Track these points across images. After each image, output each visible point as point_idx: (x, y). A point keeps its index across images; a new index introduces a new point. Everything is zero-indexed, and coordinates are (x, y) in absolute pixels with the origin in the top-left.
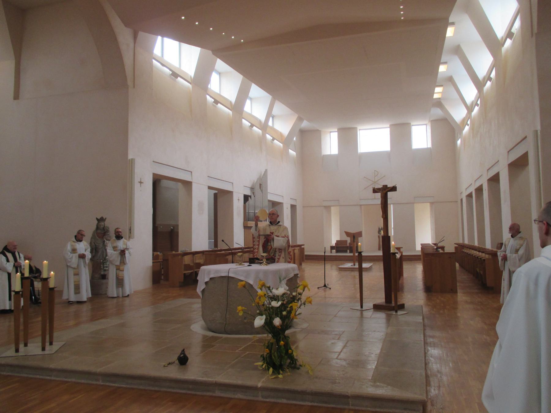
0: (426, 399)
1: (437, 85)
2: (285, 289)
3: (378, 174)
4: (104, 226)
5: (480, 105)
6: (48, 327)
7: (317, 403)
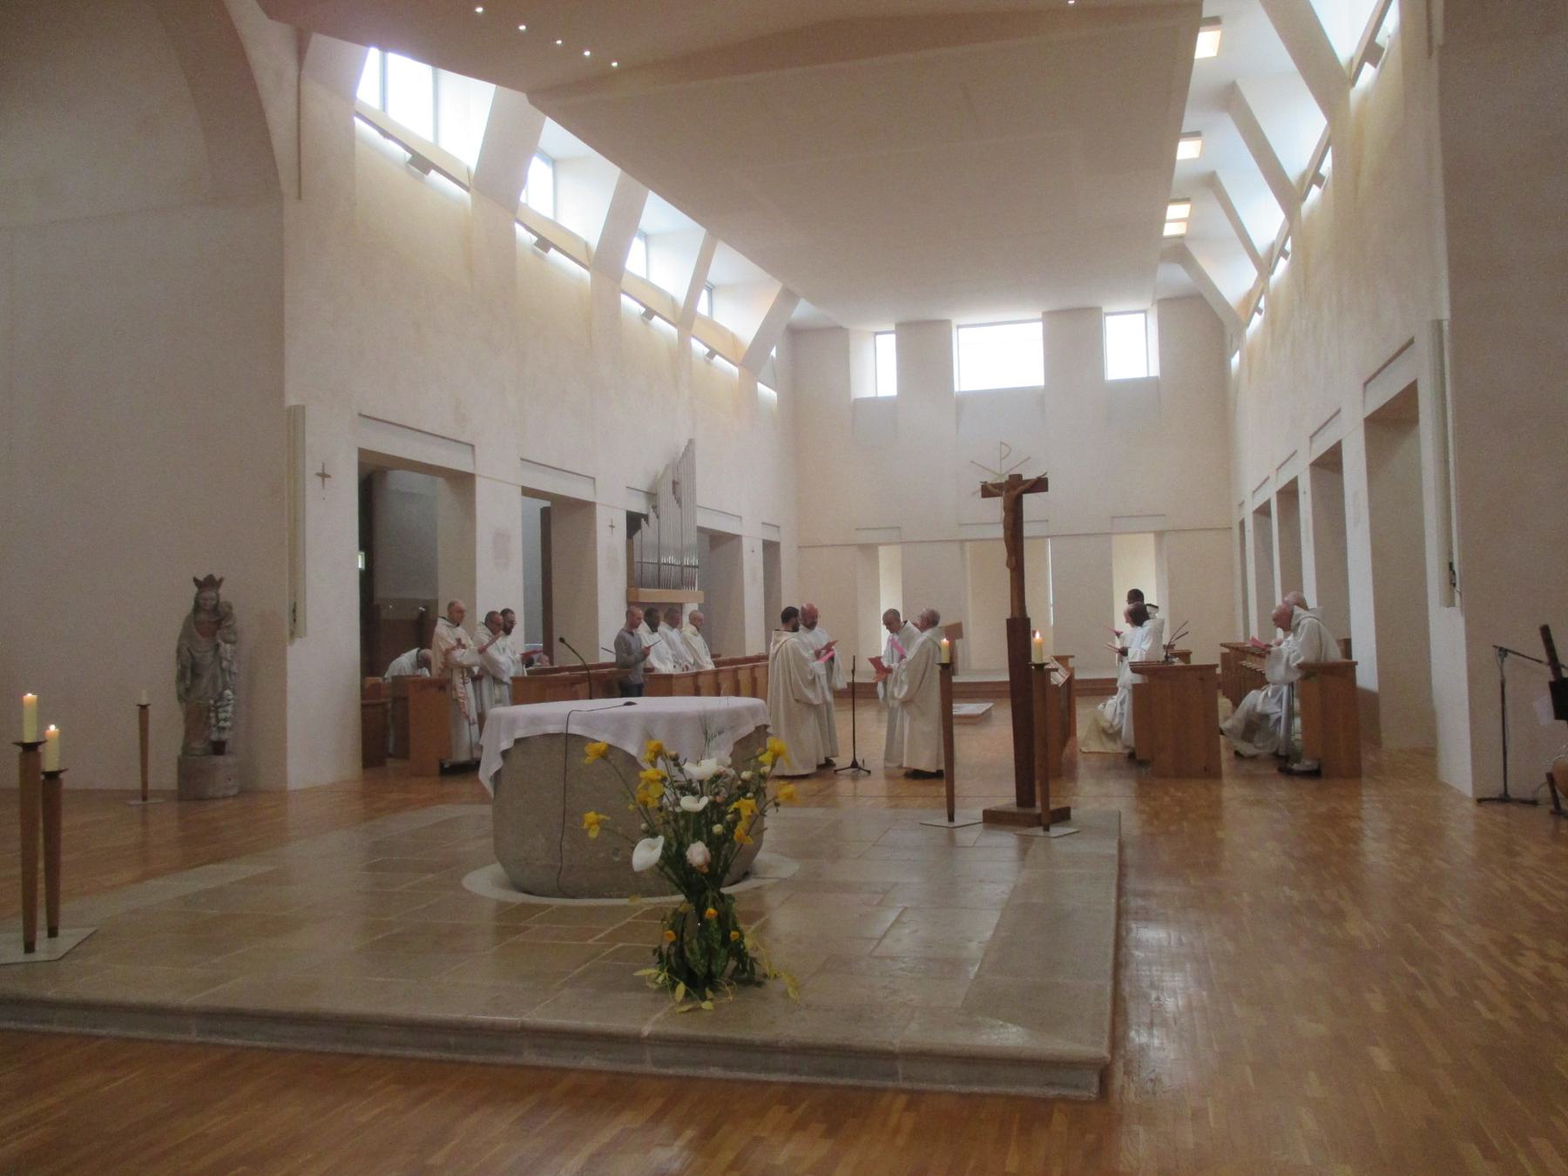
0: (1108, 1056)
2: (720, 762)
4: (218, 602)
7: (808, 1074)
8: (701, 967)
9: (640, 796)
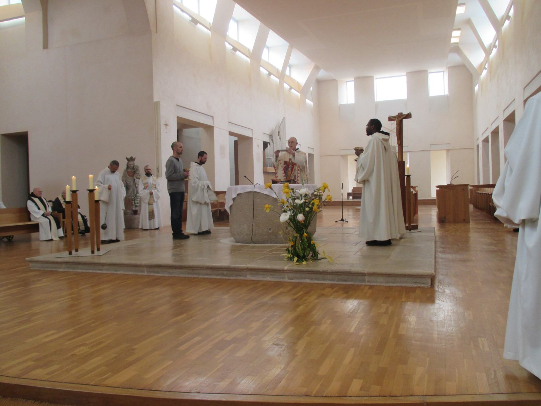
4: (134, 165)
5: (497, 47)
7: (337, 281)
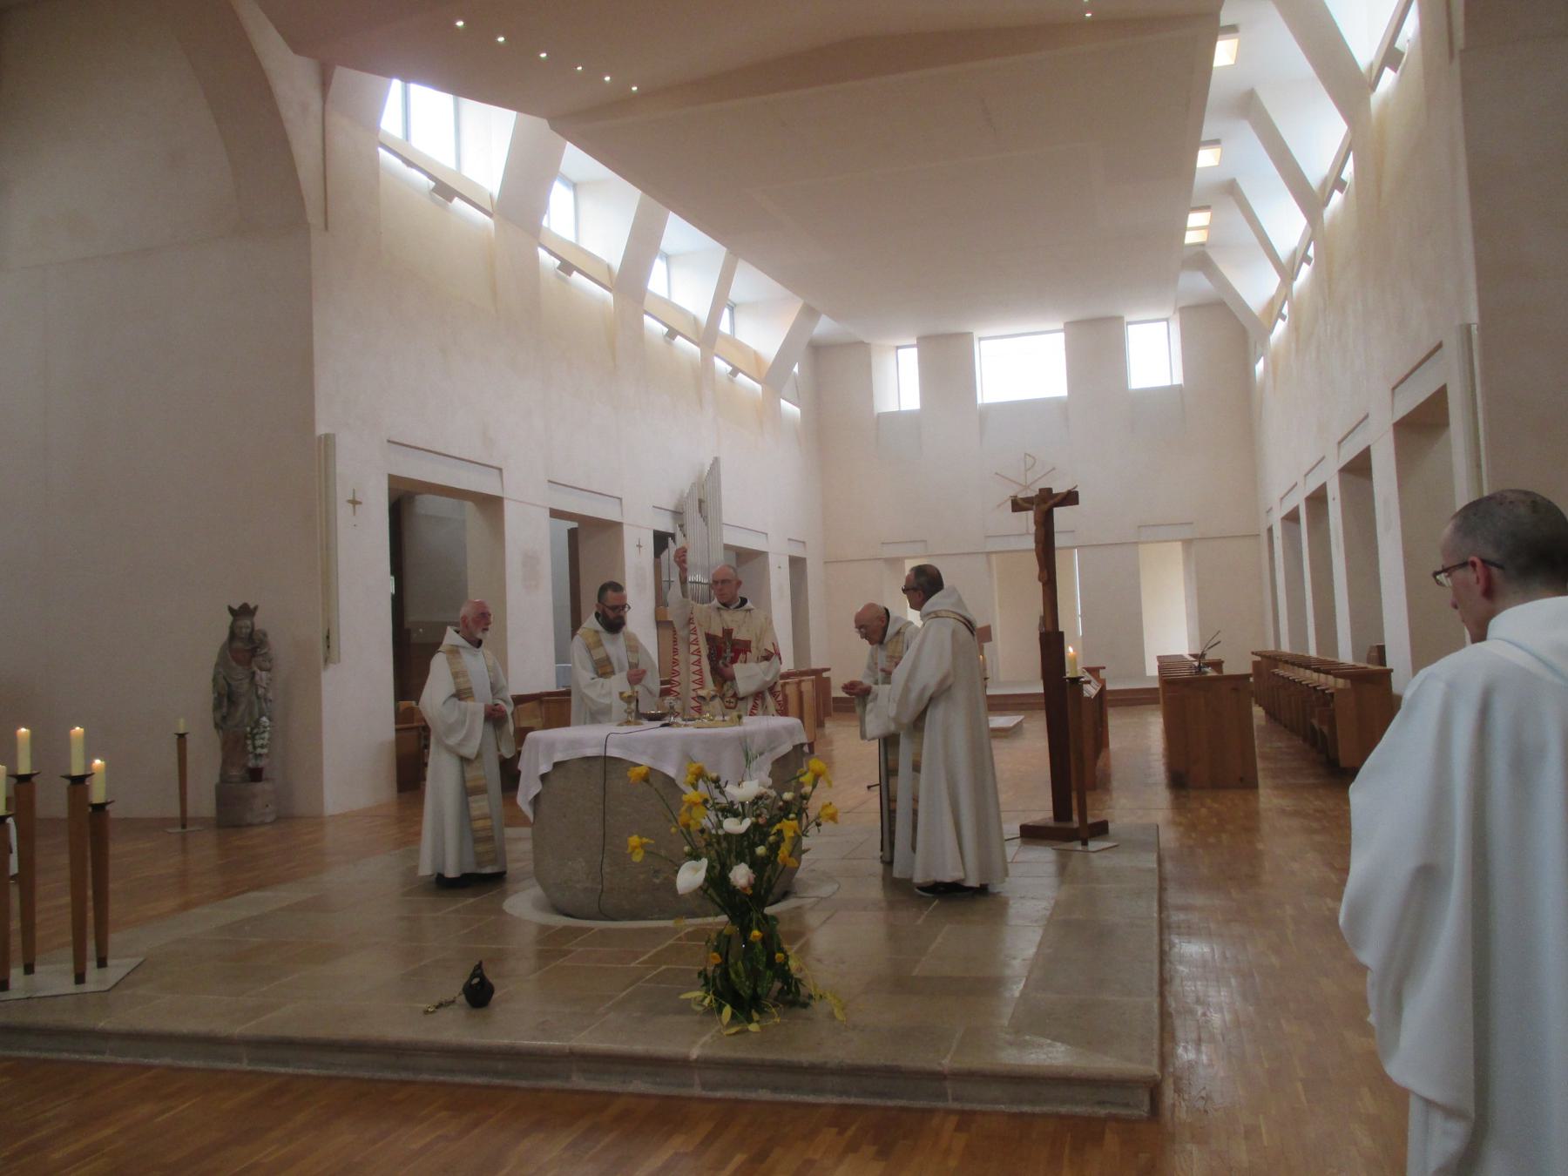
0: (1157, 1073)
1: (1192, 206)
3: (1035, 462)
4: (253, 630)
5: (1313, 261)
6: (90, 915)
7: (856, 1097)
8: (746, 989)
9: (683, 818)
